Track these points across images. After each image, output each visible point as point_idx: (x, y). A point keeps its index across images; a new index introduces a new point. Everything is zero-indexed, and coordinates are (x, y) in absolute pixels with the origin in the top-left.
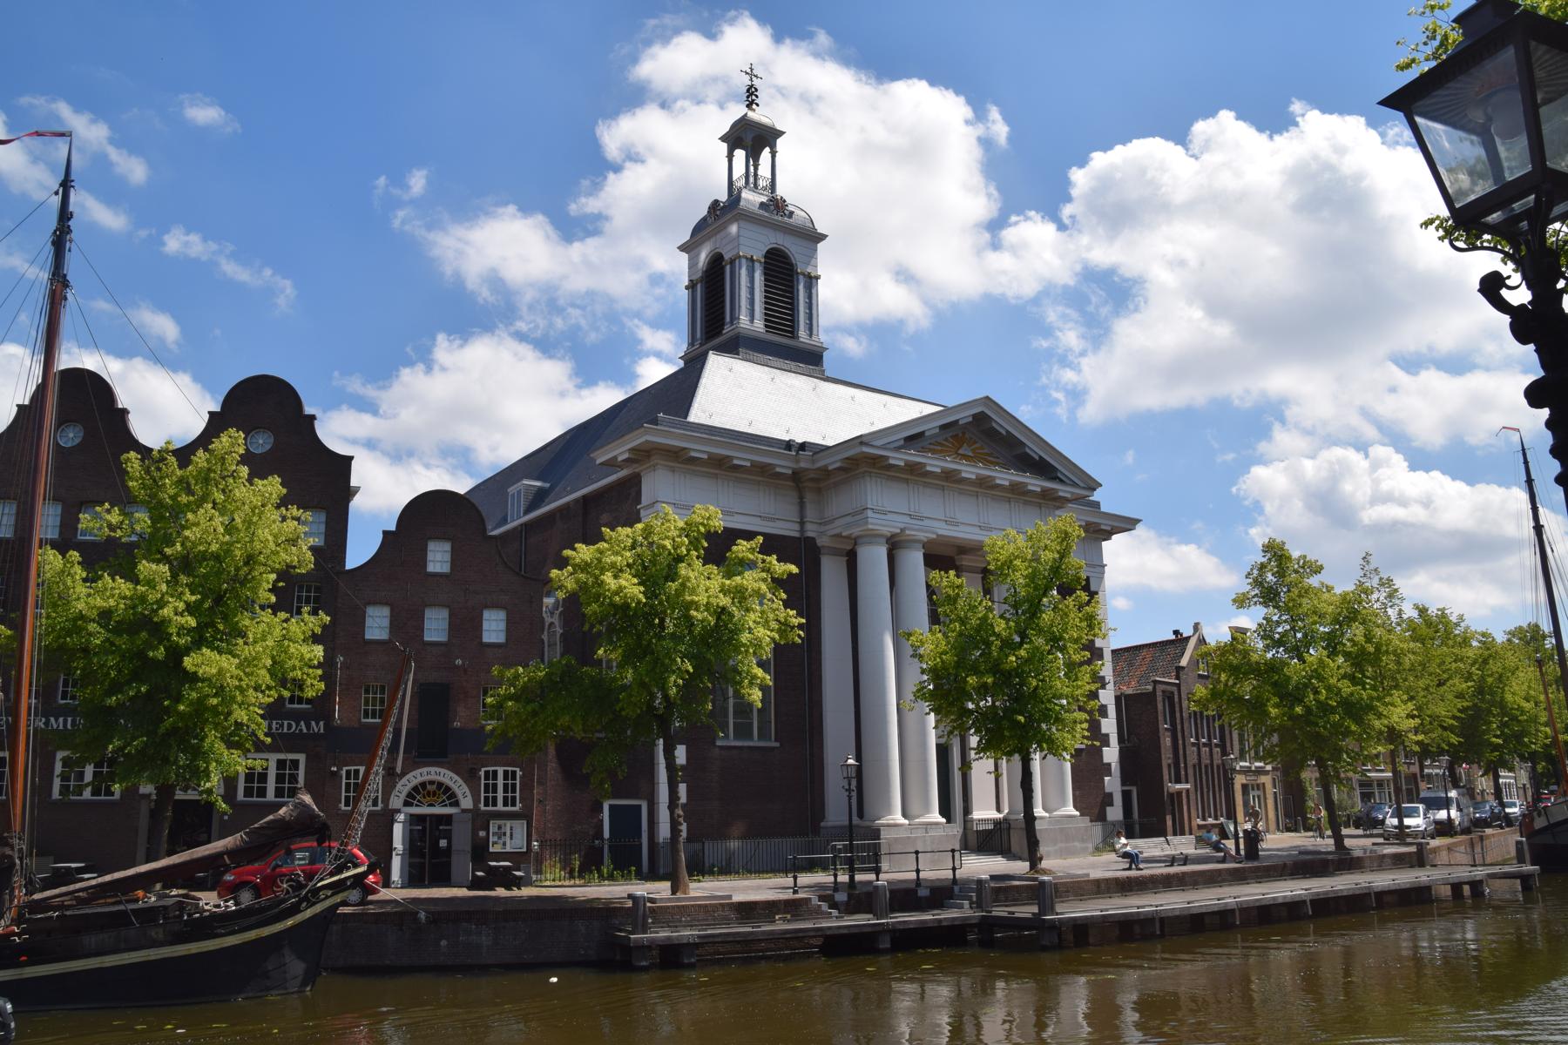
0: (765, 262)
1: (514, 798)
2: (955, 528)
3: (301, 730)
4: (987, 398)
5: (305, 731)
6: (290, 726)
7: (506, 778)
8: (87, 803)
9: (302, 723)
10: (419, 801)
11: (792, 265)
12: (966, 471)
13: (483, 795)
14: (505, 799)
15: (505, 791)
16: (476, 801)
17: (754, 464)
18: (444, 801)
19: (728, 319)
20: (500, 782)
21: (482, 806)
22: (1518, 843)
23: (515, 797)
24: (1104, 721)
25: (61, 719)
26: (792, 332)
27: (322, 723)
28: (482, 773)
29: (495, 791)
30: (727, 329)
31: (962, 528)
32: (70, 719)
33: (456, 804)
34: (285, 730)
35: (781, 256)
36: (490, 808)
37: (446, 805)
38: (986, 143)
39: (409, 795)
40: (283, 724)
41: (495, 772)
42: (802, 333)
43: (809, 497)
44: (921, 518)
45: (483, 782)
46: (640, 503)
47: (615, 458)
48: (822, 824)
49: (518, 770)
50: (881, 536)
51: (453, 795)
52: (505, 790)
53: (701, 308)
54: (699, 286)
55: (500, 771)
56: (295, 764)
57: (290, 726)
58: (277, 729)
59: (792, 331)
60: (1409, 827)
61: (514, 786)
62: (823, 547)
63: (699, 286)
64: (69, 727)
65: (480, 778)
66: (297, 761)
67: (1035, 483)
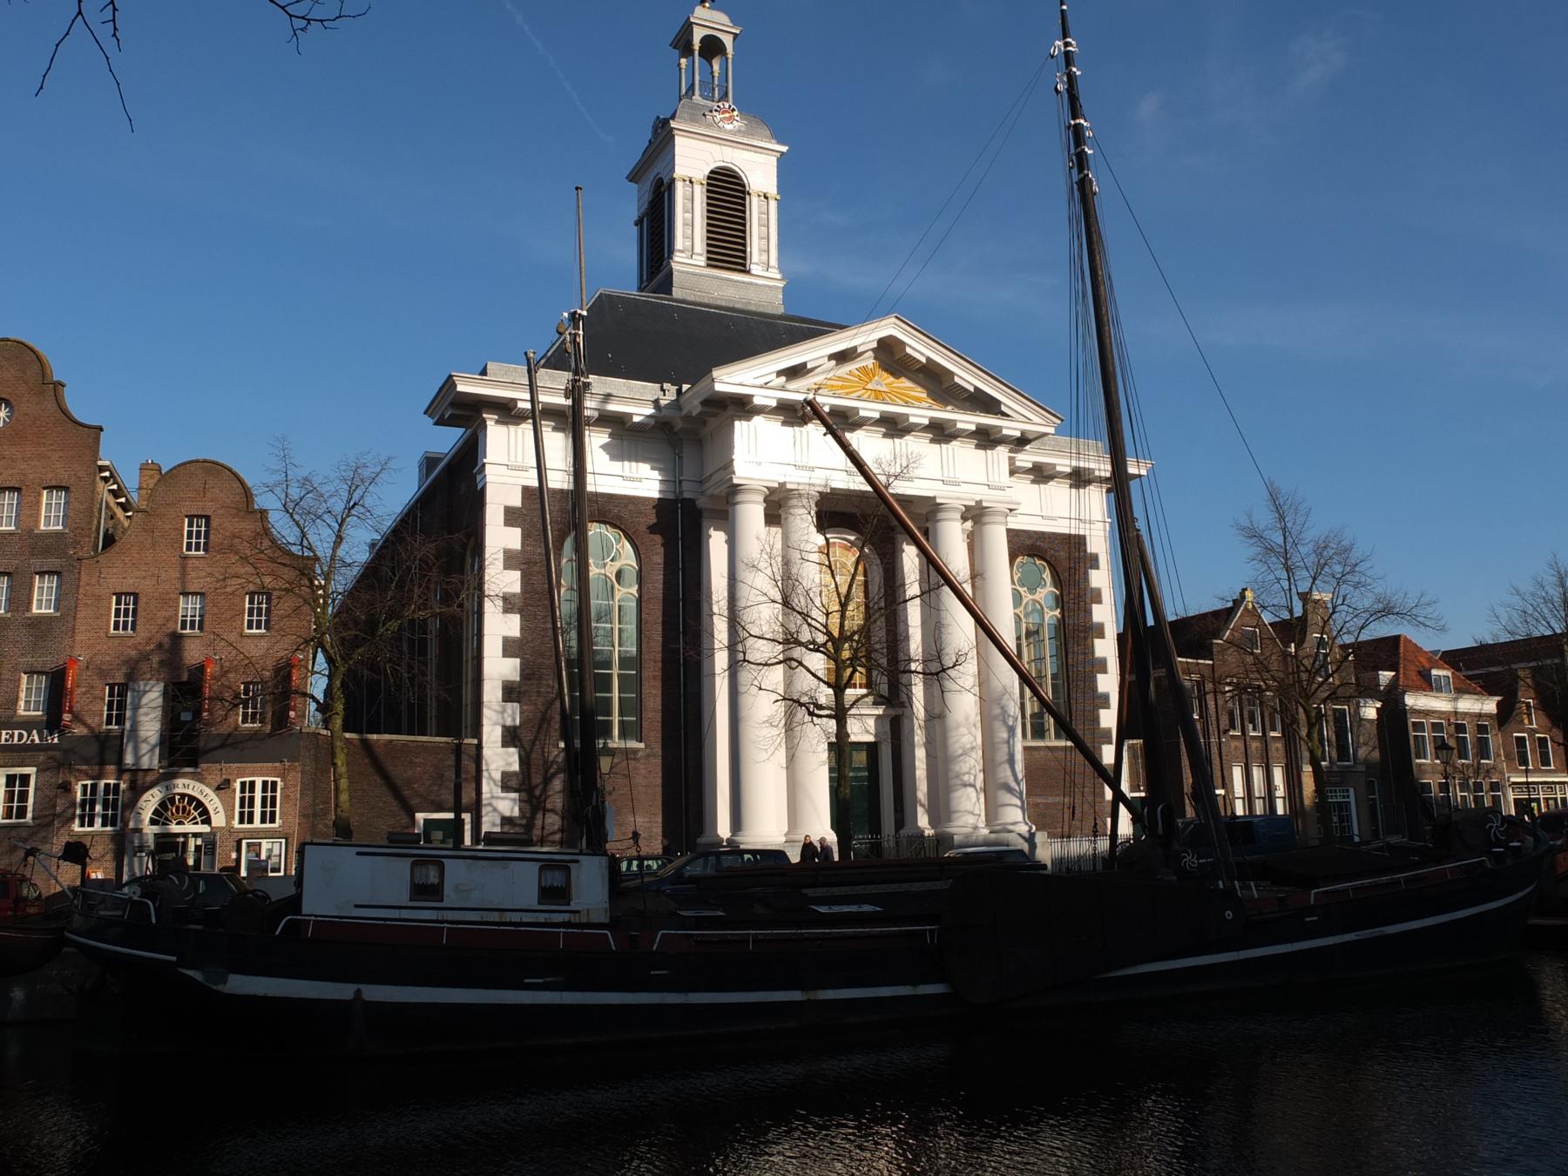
3: (33, 740)
5: (37, 741)
6: (20, 738)
7: (264, 790)
9: (35, 731)
12: (914, 415)
14: (263, 814)
15: (264, 805)
16: (229, 818)
18: (195, 818)
21: (236, 824)
22: (176, 824)
23: (275, 812)
24: (1103, 712)
26: (744, 265)
28: (237, 786)
29: (264, 799)
33: (207, 821)
36: (246, 826)
37: (197, 823)
38: (708, 8)
40: (13, 733)
41: (252, 784)
44: (957, 484)
48: (699, 840)
49: (278, 780)
51: (205, 812)
55: (259, 781)
56: (25, 779)
58: (6, 740)
61: (274, 799)
63: (645, 220)
65: (234, 790)
67: (968, 421)
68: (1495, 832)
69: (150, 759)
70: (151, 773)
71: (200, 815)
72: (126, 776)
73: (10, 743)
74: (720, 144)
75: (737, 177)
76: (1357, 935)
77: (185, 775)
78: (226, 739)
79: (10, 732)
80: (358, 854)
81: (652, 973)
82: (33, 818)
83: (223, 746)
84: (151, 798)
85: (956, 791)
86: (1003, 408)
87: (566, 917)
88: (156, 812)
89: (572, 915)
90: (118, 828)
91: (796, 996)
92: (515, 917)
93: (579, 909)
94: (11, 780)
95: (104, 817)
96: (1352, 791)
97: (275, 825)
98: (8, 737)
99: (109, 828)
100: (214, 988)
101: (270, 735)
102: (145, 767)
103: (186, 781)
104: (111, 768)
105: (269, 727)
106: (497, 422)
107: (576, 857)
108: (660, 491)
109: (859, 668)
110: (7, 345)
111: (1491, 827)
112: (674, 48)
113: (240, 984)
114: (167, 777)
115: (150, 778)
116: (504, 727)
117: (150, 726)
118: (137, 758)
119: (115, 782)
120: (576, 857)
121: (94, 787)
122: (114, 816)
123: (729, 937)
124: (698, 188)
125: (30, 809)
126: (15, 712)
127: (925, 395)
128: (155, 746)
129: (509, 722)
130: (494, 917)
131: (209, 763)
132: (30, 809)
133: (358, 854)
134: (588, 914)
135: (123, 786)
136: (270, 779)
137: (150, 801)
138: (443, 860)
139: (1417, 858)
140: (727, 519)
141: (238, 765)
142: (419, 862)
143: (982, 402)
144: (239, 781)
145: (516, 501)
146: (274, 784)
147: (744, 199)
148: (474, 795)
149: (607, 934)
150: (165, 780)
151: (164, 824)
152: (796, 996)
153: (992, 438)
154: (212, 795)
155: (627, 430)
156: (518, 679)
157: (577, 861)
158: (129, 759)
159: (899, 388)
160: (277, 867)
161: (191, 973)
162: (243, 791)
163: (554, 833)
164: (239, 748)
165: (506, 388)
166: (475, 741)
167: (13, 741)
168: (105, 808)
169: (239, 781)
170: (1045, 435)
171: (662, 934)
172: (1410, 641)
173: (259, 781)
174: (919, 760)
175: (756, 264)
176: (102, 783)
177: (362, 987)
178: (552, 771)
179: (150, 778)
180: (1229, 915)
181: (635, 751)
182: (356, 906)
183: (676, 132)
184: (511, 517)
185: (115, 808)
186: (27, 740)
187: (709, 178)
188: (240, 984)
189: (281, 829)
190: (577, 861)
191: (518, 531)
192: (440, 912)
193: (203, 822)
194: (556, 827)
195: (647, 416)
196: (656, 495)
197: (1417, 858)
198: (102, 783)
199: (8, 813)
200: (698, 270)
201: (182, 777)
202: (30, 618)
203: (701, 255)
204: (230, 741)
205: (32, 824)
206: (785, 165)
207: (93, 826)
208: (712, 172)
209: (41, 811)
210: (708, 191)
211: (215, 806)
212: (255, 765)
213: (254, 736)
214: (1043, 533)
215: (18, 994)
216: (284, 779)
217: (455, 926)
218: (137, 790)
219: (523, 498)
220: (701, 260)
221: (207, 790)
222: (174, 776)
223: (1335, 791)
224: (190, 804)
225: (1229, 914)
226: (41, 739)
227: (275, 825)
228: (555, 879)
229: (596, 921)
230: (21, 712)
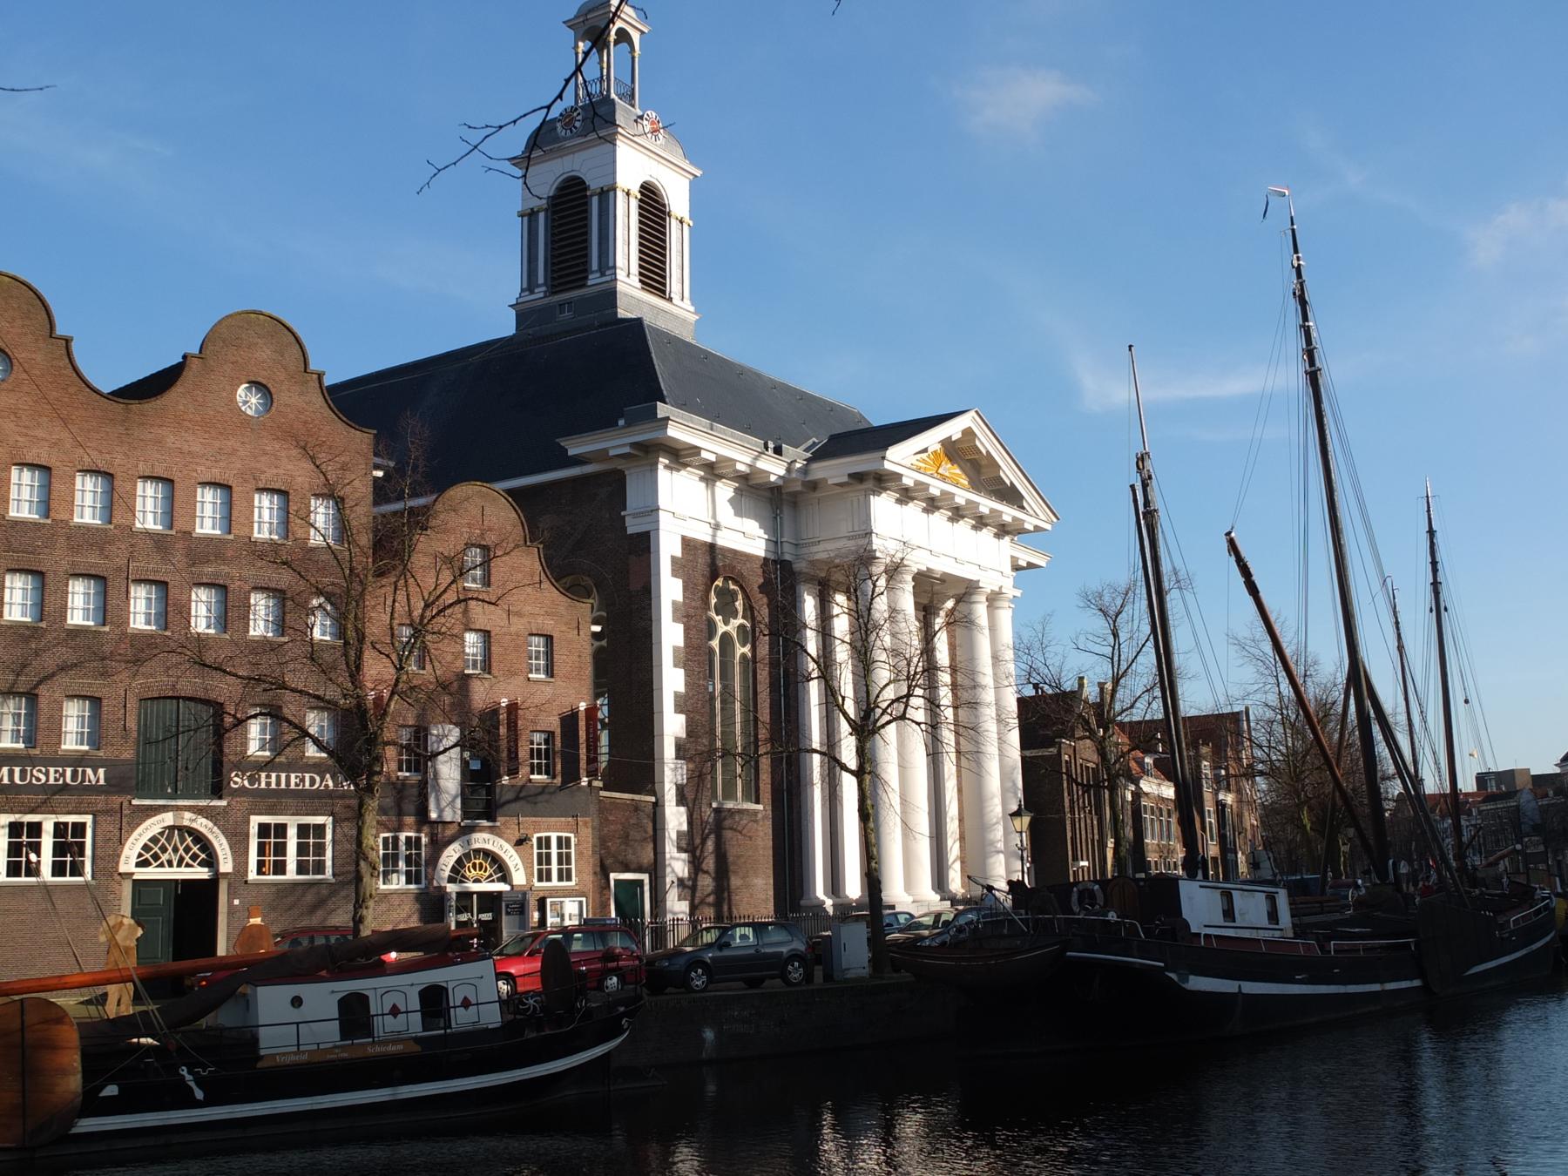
3: (327, 786)
6: (313, 782)
8: (294, 885)
9: (328, 776)
11: (664, 205)
13: (536, 867)
16: (529, 875)
18: (491, 876)
19: (595, 266)
23: (570, 869)
27: (101, 771)
30: (594, 279)
32: (17, 770)
33: (505, 877)
36: (544, 884)
37: (493, 881)
40: (304, 777)
43: (787, 513)
45: (536, 851)
46: (625, 509)
47: (606, 450)
49: (572, 835)
52: (548, 856)
53: (546, 244)
54: (542, 216)
55: (554, 836)
56: (320, 830)
58: (297, 785)
62: (800, 573)
66: (84, 825)
69: (453, 814)
70: (451, 826)
72: (426, 828)
73: (301, 787)
77: (482, 829)
78: (520, 791)
79: (60, 769)
82: (334, 875)
83: (517, 799)
84: (453, 853)
85: (991, 857)
86: (1025, 504)
88: (454, 870)
90: (423, 886)
91: (1376, 987)
94: (15, 829)
95: (408, 874)
97: (572, 883)
98: (298, 780)
99: (412, 886)
101: (561, 788)
102: (449, 820)
103: (485, 835)
104: (409, 820)
105: (558, 781)
106: (666, 467)
108: (766, 550)
110: (258, 319)
113: (1198, 983)
114: (466, 831)
115: (449, 832)
116: (676, 784)
117: (449, 772)
118: (441, 811)
119: (417, 835)
121: (396, 839)
122: (418, 873)
125: (329, 863)
127: (966, 483)
128: (455, 797)
129: (680, 782)
131: (506, 816)
132: (329, 863)
133: (1201, 887)
135: (424, 840)
136: (564, 835)
137: (451, 855)
138: (1233, 892)
141: (534, 819)
143: (1010, 495)
146: (568, 839)
147: (664, 220)
148: (652, 854)
150: (465, 834)
151: (461, 882)
152: (1376, 987)
153: (716, 472)
154: (512, 851)
155: (751, 487)
156: (684, 736)
158: (434, 815)
162: (540, 847)
163: (709, 895)
164: (529, 799)
166: (653, 799)
167: (259, 784)
168: (408, 863)
173: (554, 836)
174: (49, 833)
176: (403, 836)
177: (1242, 983)
178: (707, 831)
179: (449, 832)
181: (756, 812)
183: (619, 137)
185: (418, 864)
186: (320, 786)
188: (1198, 983)
189: (577, 888)
193: (499, 880)
194: (710, 888)
195: (780, 477)
196: (762, 554)
198: (403, 836)
199: (13, 869)
201: (480, 831)
204: (522, 795)
205: (334, 881)
206: (696, 186)
209: (343, 866)
211: (515, 863)
212: (549, 819)
213: (544, 789)
215: (709, 1035)
216: (576, 832)
218: (438, 846)
219: (683, 549)
221: (507, 846)
222: (471, 829)
226: (336, 785)
227: (572, 883)
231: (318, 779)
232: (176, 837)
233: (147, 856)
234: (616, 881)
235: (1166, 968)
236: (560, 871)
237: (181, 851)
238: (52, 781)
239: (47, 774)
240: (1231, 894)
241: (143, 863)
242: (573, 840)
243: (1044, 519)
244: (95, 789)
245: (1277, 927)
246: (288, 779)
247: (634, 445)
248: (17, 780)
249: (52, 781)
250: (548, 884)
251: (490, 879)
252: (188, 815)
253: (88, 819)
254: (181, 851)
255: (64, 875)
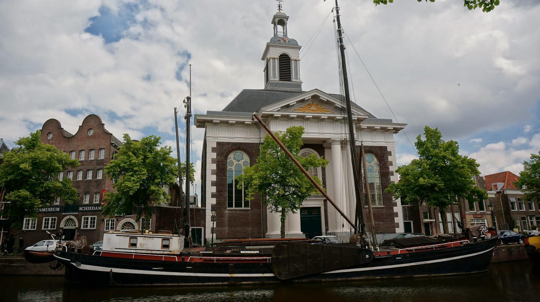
0: (279, 59)
1: (113, 227)
2: (323, 135)
4: (316, 89)
6: (94, 208)
9: (97, 207)
10: (125, 228)
12: (276, 114)
15: (111, 225)
17: (368, 127)
18: (132, 228)
20: (50, 221)
25: (45, 209)
27: (59, 208)
31: (326, 135)
33: (134, 228)
34: (93, 209)
35: (287, 56)
37: (132, 229)
39: (123, 226)
42: (293, 80)
45: (106, 223)
48: (266, 234)
49: (115, 219)
50: (338, 141)
55: (50, 218)
57: (94, 208)
59: (289, 79)
60: (63, 236)
64: (46, 211)
66: (95, 217)
68: (483, 232)
71: (133, 227)
74: (283, 48)
75: (288, 56)
76: (416, 264)
80: (116, 235)
81: (187, 267)
87: (168, 253)
89: (170, 252)
92: (155, 252)
93: (172, 250)
96: (486, 220)
100: (78, 267)
107: (171, 237)
109: (61, 185)
111: (482, 230)
112: (272, 24)
113: (84, 267)
120: (171, 237)
123: (212, 259)
124: (276, 60)
126: (93, 202)
130: (149, 252)
133: (116, 235)
134: (174, 252)
138: (170, 239)
139: (444, 240)
140: (331, 149)
142: (131, 238)
144: (106, 219)
145: (215, 146)
147: (290, 61)
149: (175, 257)
157: (172, 238)
159: (302, 110)
160: (163, 241)
161: (73, 264)
165: (226, 118)
169: (106, 219)
170: (366, 118)
171: (191, 258)
172: (511, 173)
173: (50, 218)
175: (294, 78)
180: (367, 257)
182: (116, 249)
184: (214, 150)
187: (280, 57)
188: (84, 267)
190: (172, 238)
191: (215, 154)
192: (136, 250)
197: (444, 240)
200: (278, 82)
202: (96, 180)
203: (278, 77)
207: (28, 229)
208: (281, 55)
210: (279, 60)
214: (372, 146)
217: (136, 254)
220: (277, 79)
223: (479, 220)
224: (130, 224)
225: (367, 256)
226: (98, 209)
228: (166, 243)
229: (176, 254)
230: (94, 202)
231: (94, 207)
232: (71, 220)
233: (66, 224)
234: (201, 229)
235: (71, 261)
236: (111, 227)
237: (72, 223)
238: (51, 211)
239: (51, 209)
240: (137, 238)
241: (65, 226)
242: (115, 220)
243: (317, 113)
244: (57, 212)
245: (136, 249)
246: (89, 208)
247: (367, 127)
248: (46, 211)
249: (51, 211)
250: (28, 229)
251: (131, 228)
252: (71, 216)
253: (56, 218)
254: (70, 223)
255: (91, 228)
